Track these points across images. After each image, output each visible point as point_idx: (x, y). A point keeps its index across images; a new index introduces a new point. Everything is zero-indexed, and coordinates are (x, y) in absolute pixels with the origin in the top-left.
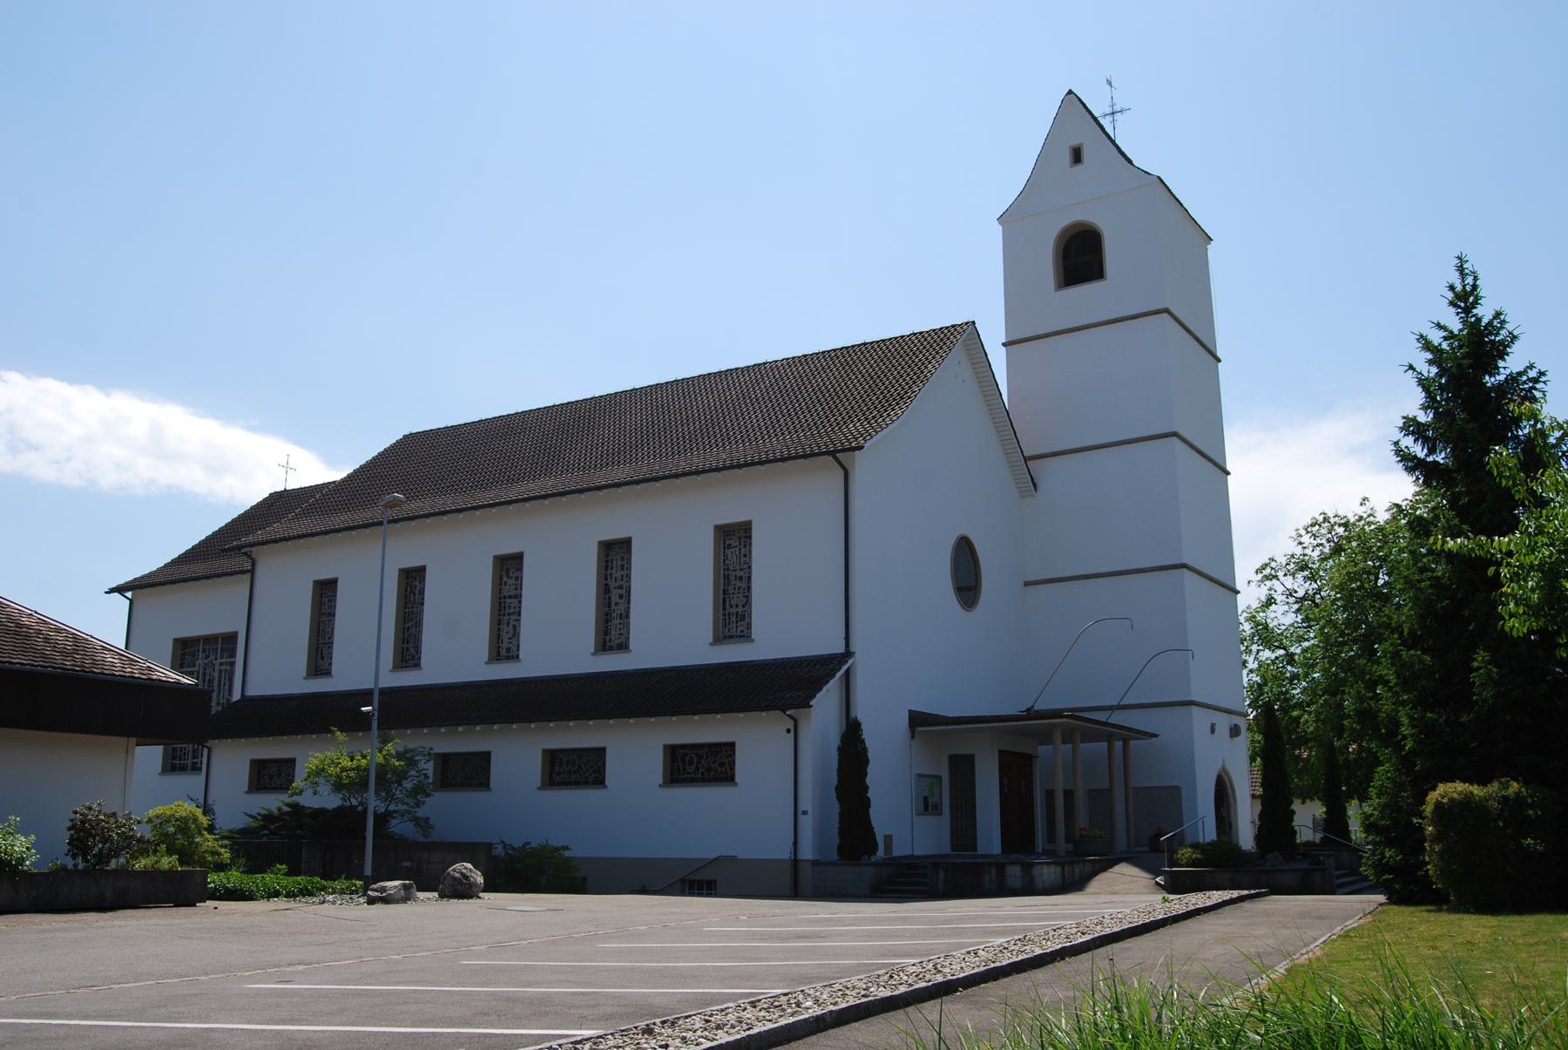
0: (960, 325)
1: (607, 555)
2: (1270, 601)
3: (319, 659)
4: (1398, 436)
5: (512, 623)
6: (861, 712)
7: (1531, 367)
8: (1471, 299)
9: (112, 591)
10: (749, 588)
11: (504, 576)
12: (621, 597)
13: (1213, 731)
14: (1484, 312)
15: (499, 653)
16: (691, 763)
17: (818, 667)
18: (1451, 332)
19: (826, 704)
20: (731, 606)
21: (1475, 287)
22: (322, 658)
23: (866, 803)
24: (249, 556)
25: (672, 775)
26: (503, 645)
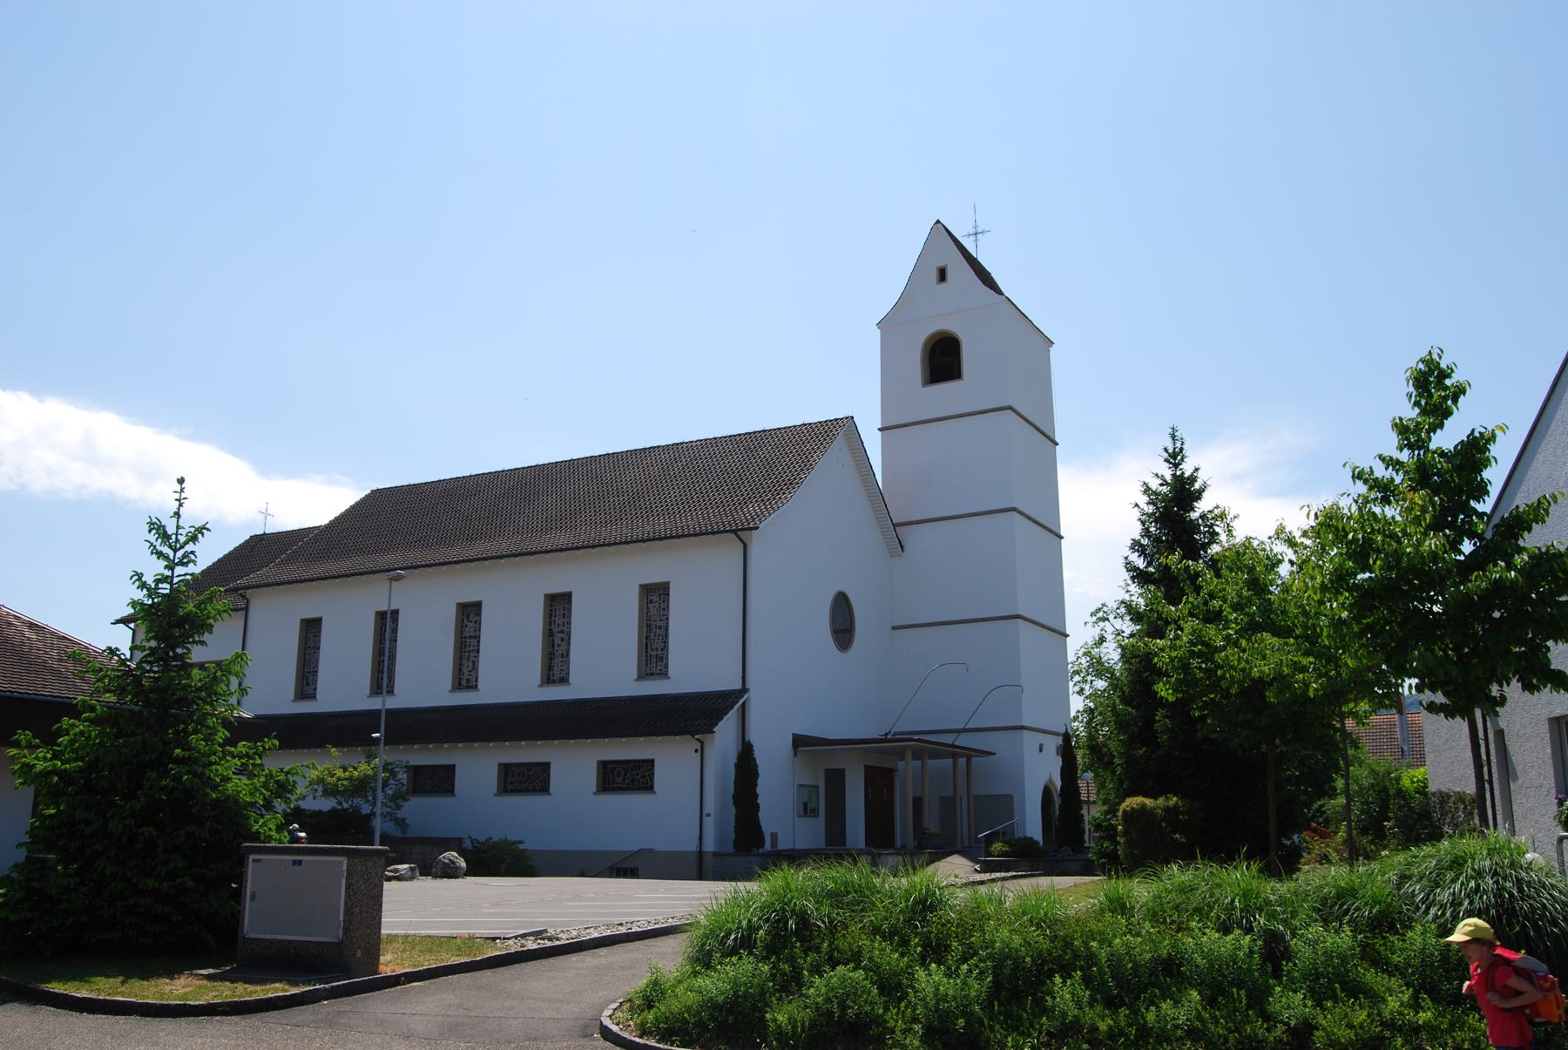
0: (841, 419)
1: (551, 606)
2: (1102, 640)
3: (306, 684)
4: (1127, 552)
5: (471, 658)
6: (753, 737)
7: (1217, 507)
8: (1179, 458)
9: (118, 622)
10: (667, 635)
11: (465, 621)
12: (562, 639)
13: (1041, 750)
14: (1187, 468)
15: (460, 683)
16: (619, 775)
17: (720, 700)
18: (1165, 481)
19: (725, 732)
20: (652, 650)
21: (1181, 449)
22: (308, 684)
23: (757, 808)
24: (244, 597)
25: (603, 784)
26: (465, 676)
